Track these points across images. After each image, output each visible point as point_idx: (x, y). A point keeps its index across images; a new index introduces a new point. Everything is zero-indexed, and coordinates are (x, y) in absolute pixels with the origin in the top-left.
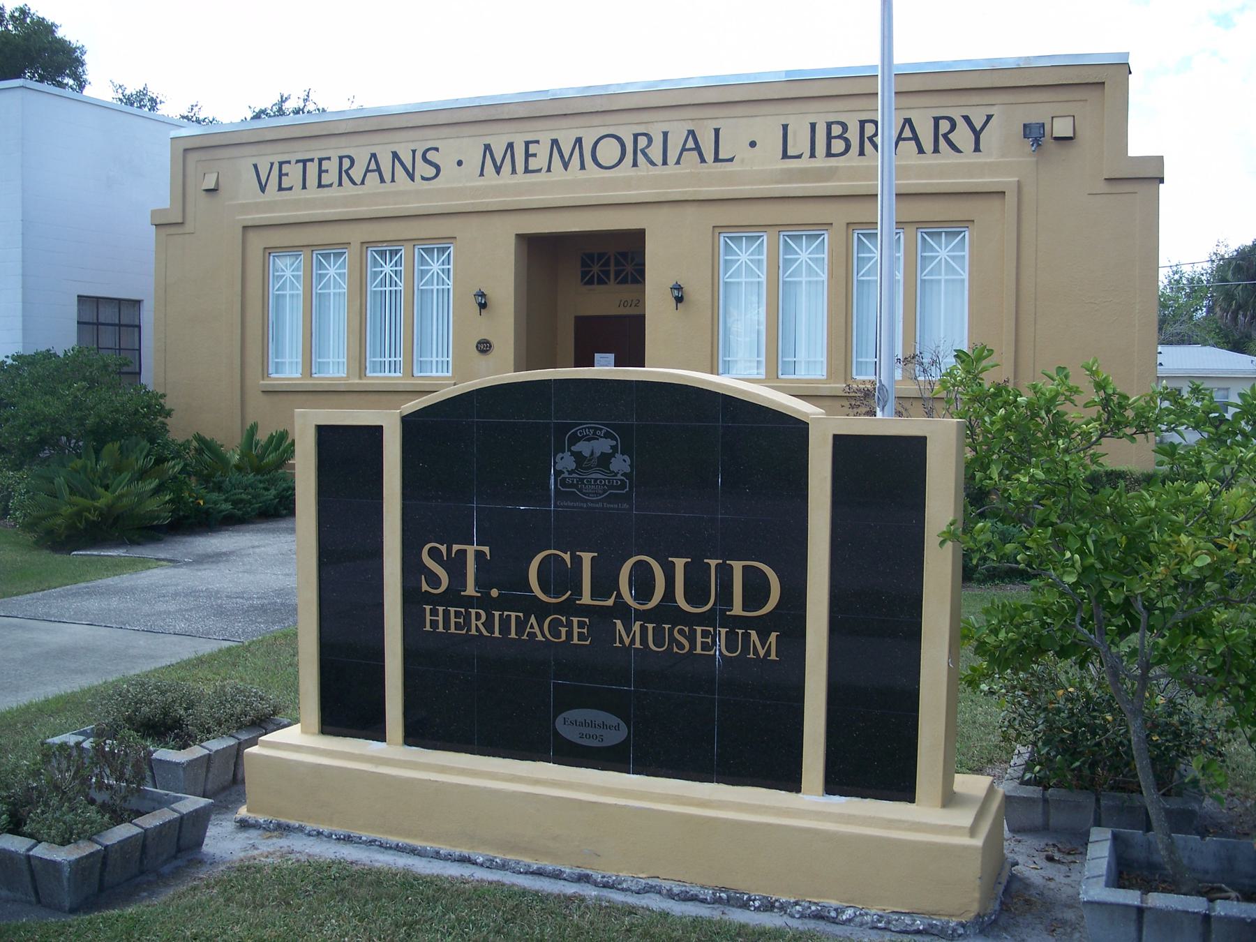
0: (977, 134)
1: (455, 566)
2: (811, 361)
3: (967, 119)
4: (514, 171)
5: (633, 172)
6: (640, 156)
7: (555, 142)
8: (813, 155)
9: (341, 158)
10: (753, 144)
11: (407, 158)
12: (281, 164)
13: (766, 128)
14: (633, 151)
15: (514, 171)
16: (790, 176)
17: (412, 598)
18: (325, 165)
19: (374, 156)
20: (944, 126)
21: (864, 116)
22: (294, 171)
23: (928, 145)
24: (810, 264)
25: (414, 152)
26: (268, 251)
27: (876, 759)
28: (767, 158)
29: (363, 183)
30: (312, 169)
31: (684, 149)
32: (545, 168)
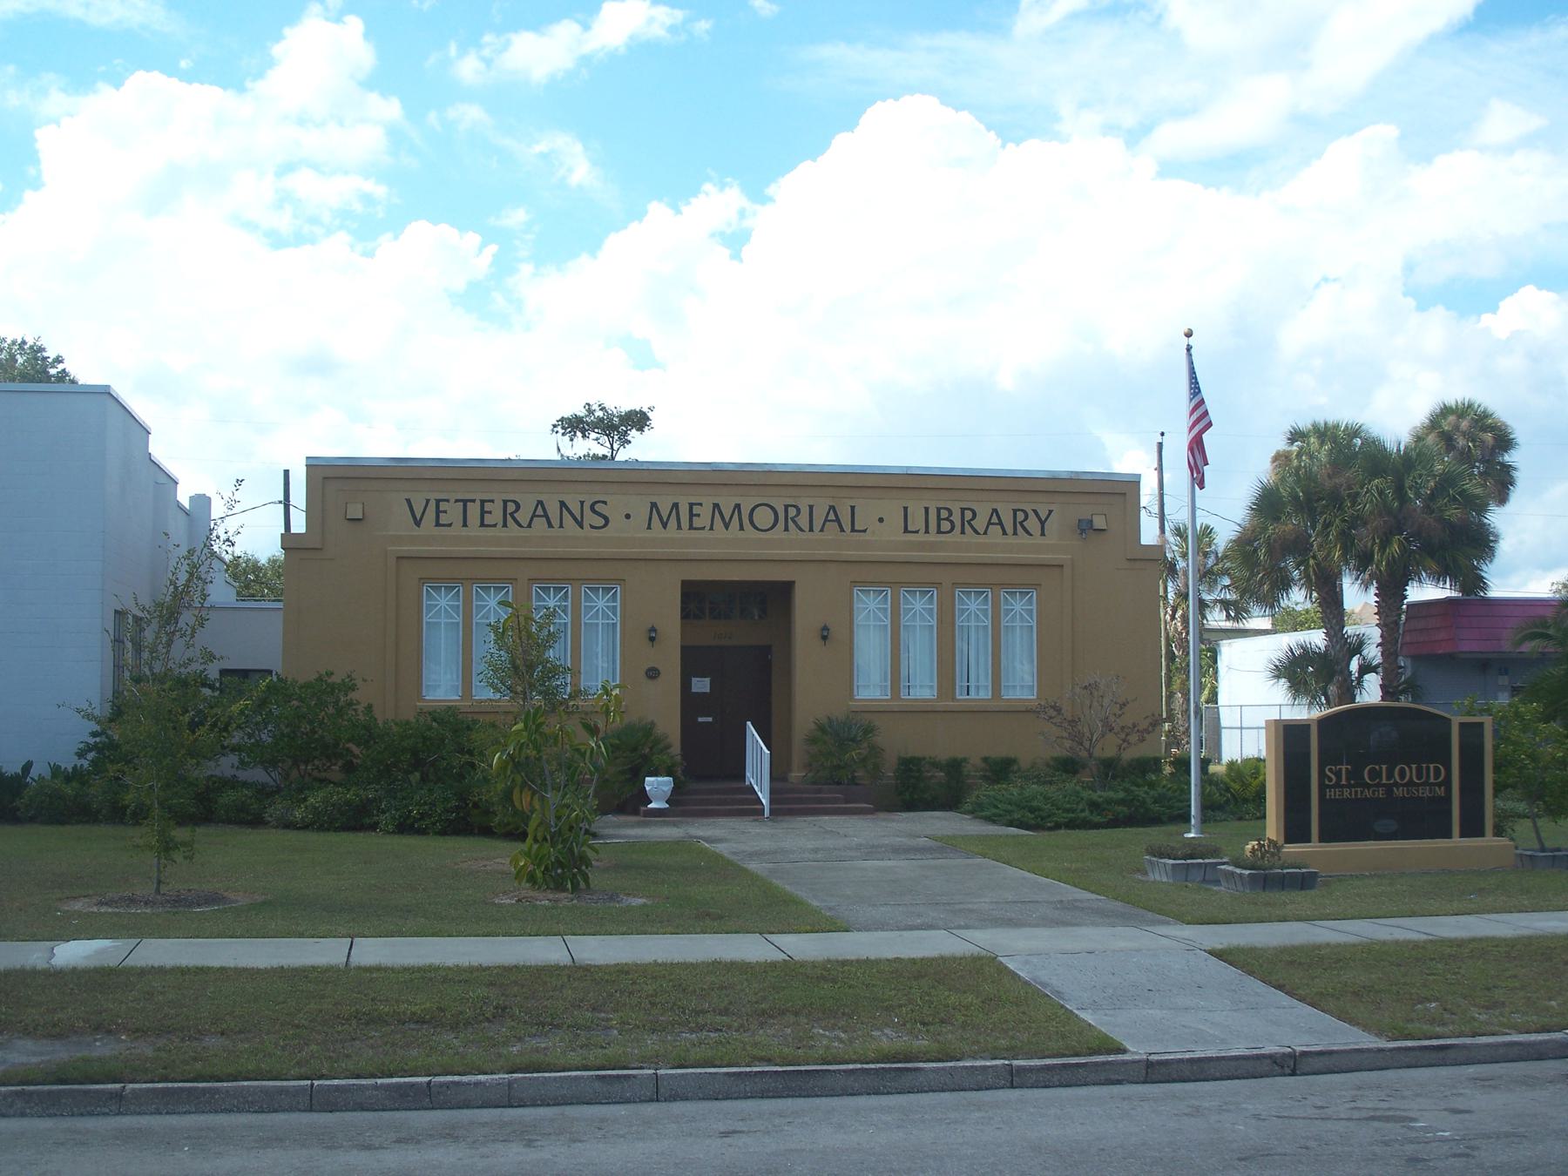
0: (1043, 523)
1: (1338, 774)
2: (1022, 682)
4: (679, 527)
5: (784, 535)
6: (790, 523)
7: (716, 506)
8: (927, 532)
9: (505, 502)
12: (438, 502)
13: (891, 509)
15: (679, 527)
17: (1322, 787)
18: (488, 507)
20: (1020, 516)
23: (1010, 530)
24: (920, 609)
25: (582, 503)
26: (423, 580)
27: (1472, 827)
28: (891, 532)
29: (529, 526)
30: (473, 510)
31: (826, 520)
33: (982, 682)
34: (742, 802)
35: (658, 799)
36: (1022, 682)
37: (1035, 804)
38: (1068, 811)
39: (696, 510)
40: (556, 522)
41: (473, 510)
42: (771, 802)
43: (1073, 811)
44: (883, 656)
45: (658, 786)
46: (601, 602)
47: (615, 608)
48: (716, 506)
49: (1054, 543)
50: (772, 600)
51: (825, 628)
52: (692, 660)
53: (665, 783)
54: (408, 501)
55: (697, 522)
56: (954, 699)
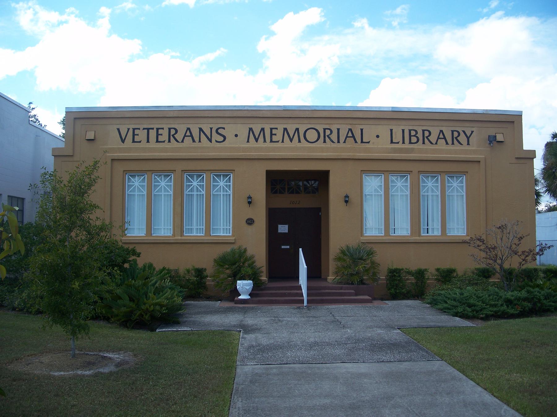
0: (468, 138)
2: (458, 229)
4: (265, 141)
5: (324, 145)
6: (327, 138)
7: (285, 129)
8: (403, 143)
9: (170, 129)
12: (134, 129)
13: (383, 130)
15: (265, 141)
20: (456, 134)
23: (450, 141)
24: (401, 187)
25: (211, 129)
28: (384, 143)
29: (183, 141)
30: (153, 134)
31: (347, 137)
33: (435, 226)
34: (290, 295)
35: (244, 293)
36: (458, 229)
37: (472, 301)
38: (492, 306)
39: (274, 131)
40: (197, 139)
41: (153, 134)
42: (308, 295)
43: (495, 306)
44: (379, 213)
45: (244, 286)
46: (222, 183)
47: (230, 185)
48: (285, 129)
49: (475, 149)
50: (316, 181)
51: (347, 196)
52: (274, 216)
53: (247, 285)
54: (118, 130)
55: (275, 138)
56: (420, 235)
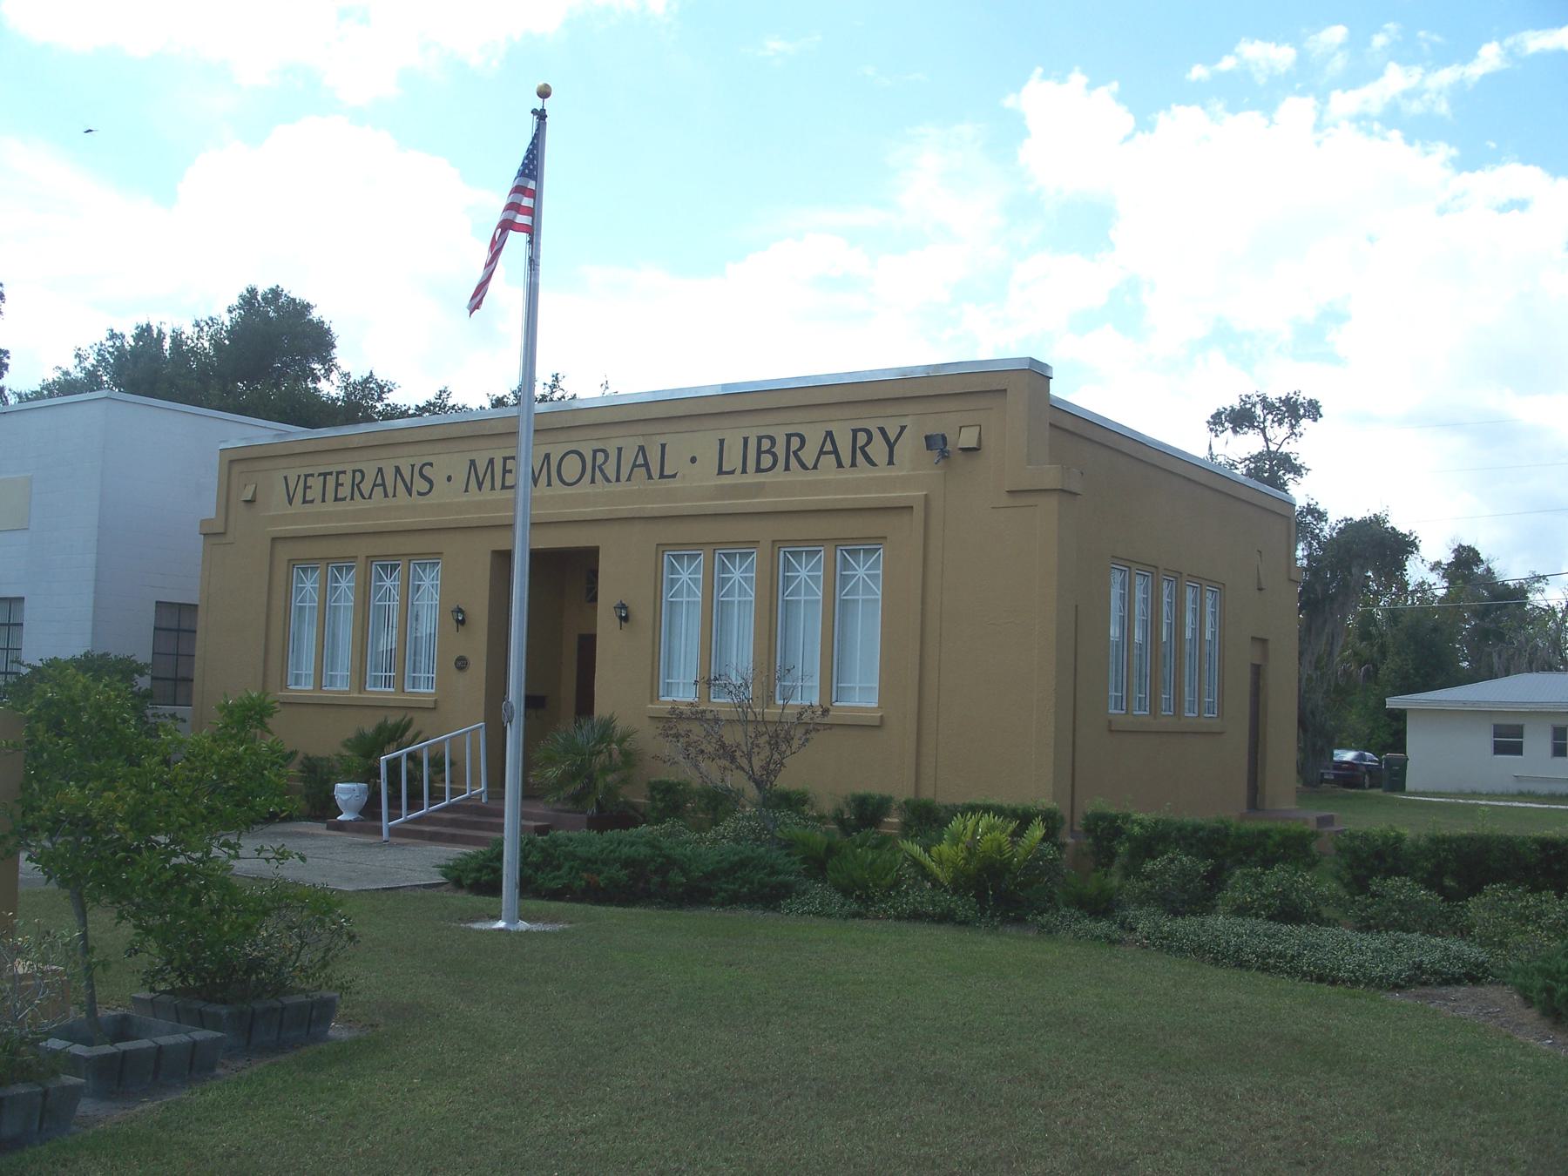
0: (891, 446)
3: (882, 430)
4: (493, 488)
5: (590, 489)
6: (793, 459)
8: (744, 471)
10: (693, 460)
11: (482, 466)
13: (703, 443)
14: (593, 468)
15: (493, 488)
16: (724, 492)
19: (829, 434)
21: (790, 430)
22: (316, 483)
23: (846, 460)
26: (292, 563)
29: (815, 467)
30: (331, 480)
31: (634, 466)
32: (739, 470)
